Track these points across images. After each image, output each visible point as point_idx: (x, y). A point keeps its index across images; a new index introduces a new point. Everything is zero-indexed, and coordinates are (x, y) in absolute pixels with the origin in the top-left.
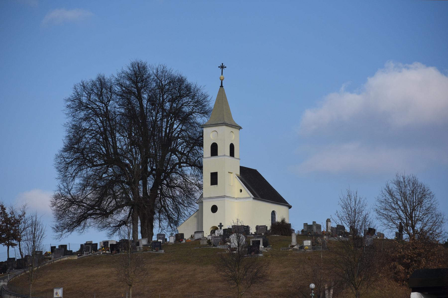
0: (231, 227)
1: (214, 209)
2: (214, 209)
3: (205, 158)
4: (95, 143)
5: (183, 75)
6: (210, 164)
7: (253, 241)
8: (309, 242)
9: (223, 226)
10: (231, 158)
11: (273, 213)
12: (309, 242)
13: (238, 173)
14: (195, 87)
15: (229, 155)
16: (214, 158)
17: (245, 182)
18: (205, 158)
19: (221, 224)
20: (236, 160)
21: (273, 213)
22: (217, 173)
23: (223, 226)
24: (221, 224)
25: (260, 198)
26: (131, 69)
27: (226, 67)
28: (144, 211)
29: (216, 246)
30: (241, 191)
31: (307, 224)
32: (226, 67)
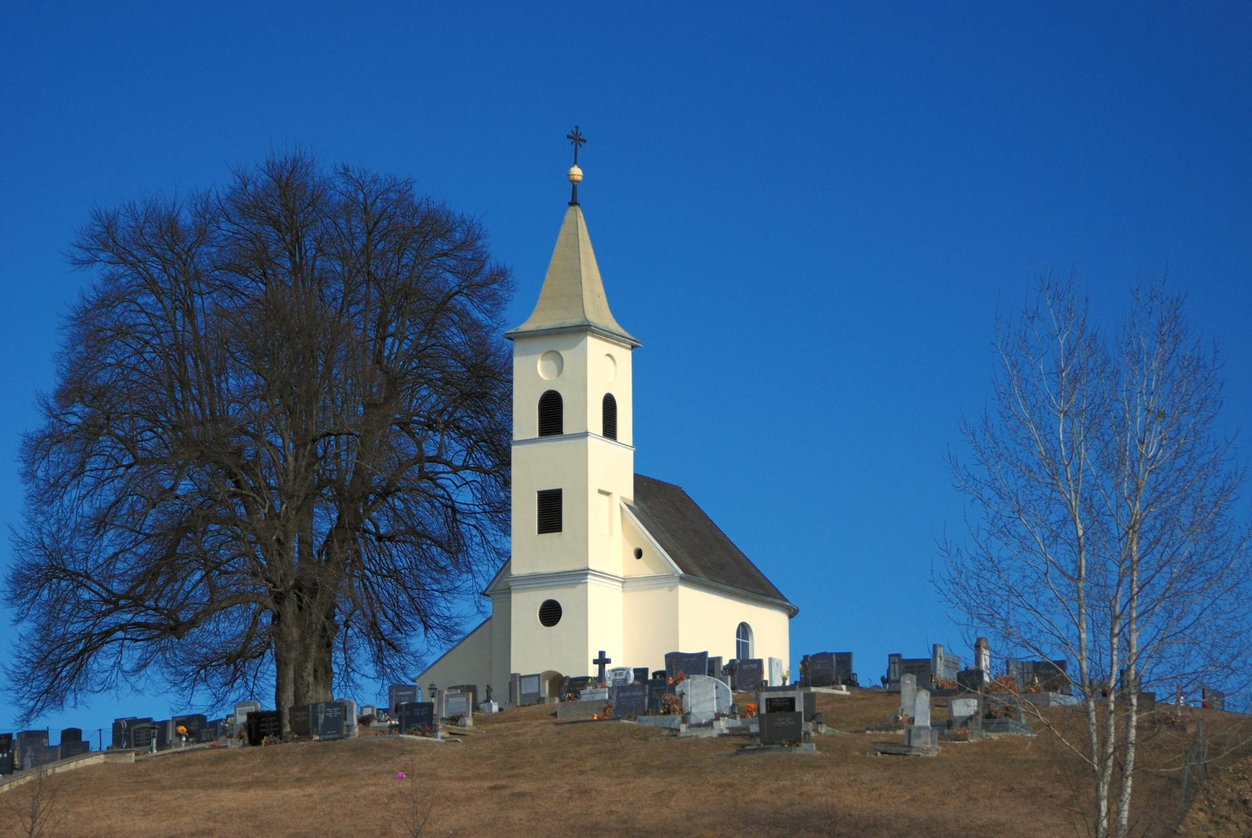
1: (551, 614)
2: (551, 614)
3: (520, 442)
5: (10, 662)
6: (532, 466)
7: (769, 701)
9: (608, 661)
10: (608, 443)
11: (744, 631)
13: (630, 495)
15: (600, 432)
16: (552, 446)
18: (520, 442)
19: (602, 654)
20: (621, 449)
21: (744, 631)
23: (608, 661)
24: (602, 654)
25: (704, 579)
27: (569, 137)
30: (639, 554)
31: (899, 655)
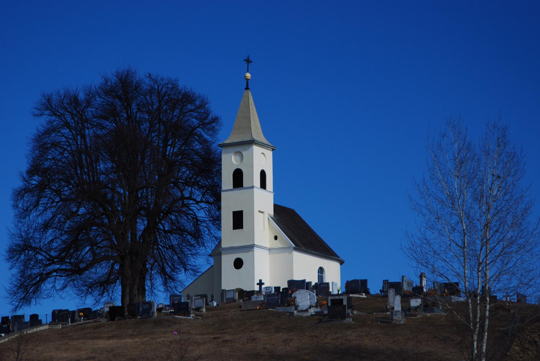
0: (39, 319)
1: (238, 264)
2: (238, 264)
4: (40, 156)
6: (230, 201)
8: (419, 300)
9: (263, 284)
10: (262, 191)
12: (419, 300)
13: (272, 213)
14: (193, 96)
15: (259, 186)
17: (65, 312)
19: (260, 281)
22: (242, 211)
23: (263, 284)
24: (260, 281)
25: (304, 249)
26: (87, 92)
27: (245, 60)
28: (133, 267)
29: (432, 311)
30: (276, 238)
32: (245, 60)
